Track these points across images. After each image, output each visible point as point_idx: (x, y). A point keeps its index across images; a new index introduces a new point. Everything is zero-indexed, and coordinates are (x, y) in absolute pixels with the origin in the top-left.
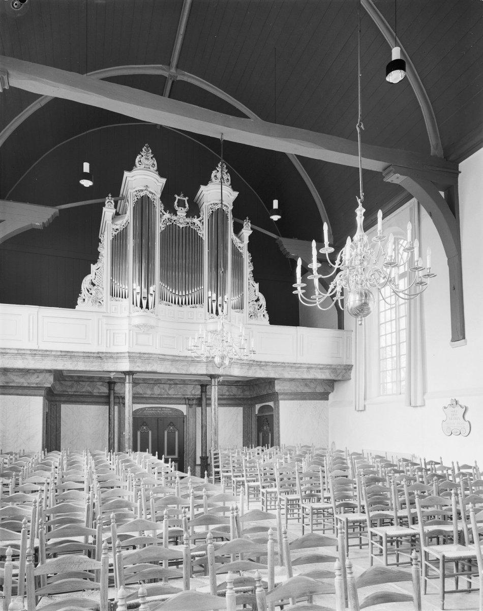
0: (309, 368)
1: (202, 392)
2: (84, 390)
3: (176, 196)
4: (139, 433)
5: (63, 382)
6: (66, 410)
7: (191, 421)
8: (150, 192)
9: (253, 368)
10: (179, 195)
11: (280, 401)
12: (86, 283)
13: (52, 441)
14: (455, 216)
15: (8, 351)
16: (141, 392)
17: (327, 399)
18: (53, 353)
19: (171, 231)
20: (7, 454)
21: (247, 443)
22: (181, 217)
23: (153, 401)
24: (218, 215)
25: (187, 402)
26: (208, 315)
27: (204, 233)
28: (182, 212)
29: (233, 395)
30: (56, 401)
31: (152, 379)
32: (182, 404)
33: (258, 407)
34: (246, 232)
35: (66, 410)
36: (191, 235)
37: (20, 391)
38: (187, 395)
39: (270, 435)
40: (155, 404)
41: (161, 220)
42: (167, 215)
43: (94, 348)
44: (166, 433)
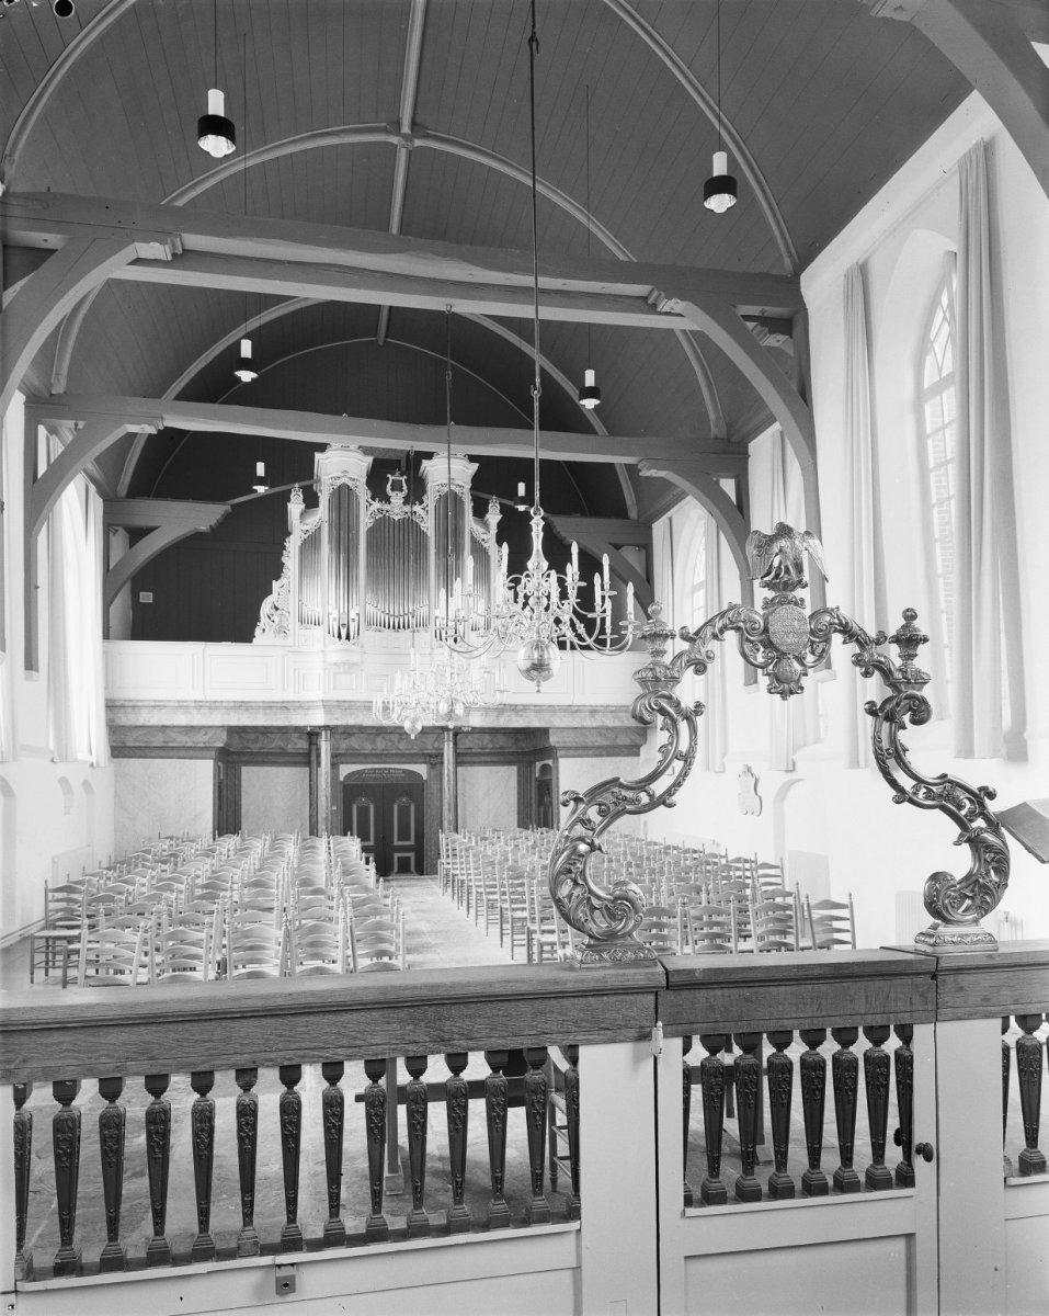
0: (593, 711)
3: (389, 476)
5: (243, 735)
6: (251, 776)
7: (435, 787)
8: (351, 479)
9: (506, 714)
10: (392, 475)
11: (561, 760)
12: (266, 607)
13: (228, 819)
14: (742, 513)
15: (167, 704)
16: (357, 747)
17: (637, 754)
18: (224, 704)
19: (381, 526)
20: (167, 838)
21: (523, 823)
22: (397, 506)
23: (375, 760)
24: (450, 502)
26: (436, 642)
27: (429, 525)
28: (397, 498)
29: (501, 748)
30: (233, 762)
32: (421, 763)
33: (538, 765)
34: (494, 517)
35: (251, 776)
36: (410, 526)
37: (182, 753)
40: (378, 763)
41: (367, 513)
42: (376, 505)
43: (278, 697)
44: (396, 807)
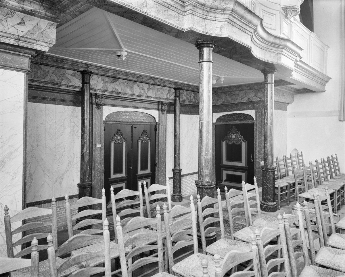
1: (176, 96)
2: (47, 79)
4: (224, 144)
16: (120, 91)
25: (160, 107)
31: (134, 74)
38: (163, 99)
39: (244, 145)
44: (140, 143)
